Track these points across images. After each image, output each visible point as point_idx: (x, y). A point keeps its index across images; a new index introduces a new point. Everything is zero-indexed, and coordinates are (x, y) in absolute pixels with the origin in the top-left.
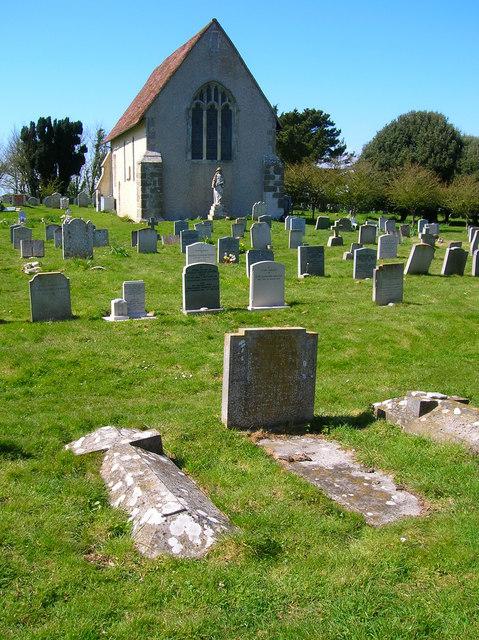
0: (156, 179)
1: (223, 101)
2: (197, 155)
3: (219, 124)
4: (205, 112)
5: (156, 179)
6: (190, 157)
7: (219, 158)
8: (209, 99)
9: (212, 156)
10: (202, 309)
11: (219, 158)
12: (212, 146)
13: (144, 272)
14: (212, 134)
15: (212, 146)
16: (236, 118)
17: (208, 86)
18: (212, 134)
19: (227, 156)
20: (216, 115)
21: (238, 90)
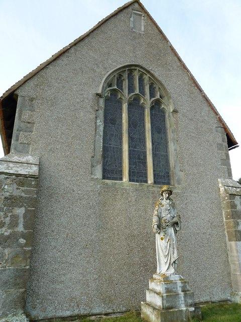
0: (20, 211)
1: (152, 95)
2: (111, 171)
3: (148, 125)
4: (125, 107)
5: (20, 211)
6: (98, 173)
7: (151, 180)
8: (131, 89)
9: (138, 175)
10: (176, 255)
11: (151, 180)
12: (138, 159)
13: (153, 316)
14: (137, 142)
15: (138, 159)
16: (173, 119)
17: (130, 69)
18: (137, 142)
19: (163, 177)
20: (143, 114)
21: (171, 84)
